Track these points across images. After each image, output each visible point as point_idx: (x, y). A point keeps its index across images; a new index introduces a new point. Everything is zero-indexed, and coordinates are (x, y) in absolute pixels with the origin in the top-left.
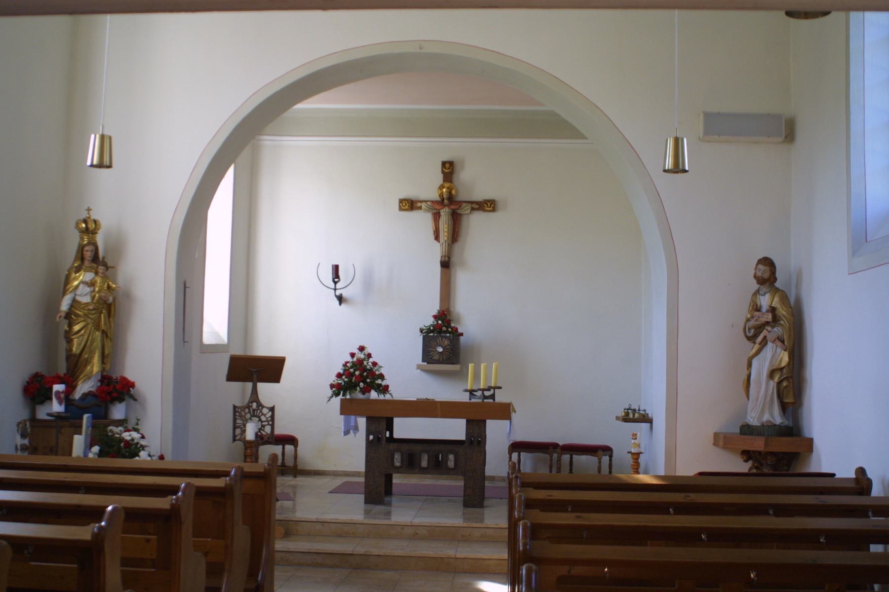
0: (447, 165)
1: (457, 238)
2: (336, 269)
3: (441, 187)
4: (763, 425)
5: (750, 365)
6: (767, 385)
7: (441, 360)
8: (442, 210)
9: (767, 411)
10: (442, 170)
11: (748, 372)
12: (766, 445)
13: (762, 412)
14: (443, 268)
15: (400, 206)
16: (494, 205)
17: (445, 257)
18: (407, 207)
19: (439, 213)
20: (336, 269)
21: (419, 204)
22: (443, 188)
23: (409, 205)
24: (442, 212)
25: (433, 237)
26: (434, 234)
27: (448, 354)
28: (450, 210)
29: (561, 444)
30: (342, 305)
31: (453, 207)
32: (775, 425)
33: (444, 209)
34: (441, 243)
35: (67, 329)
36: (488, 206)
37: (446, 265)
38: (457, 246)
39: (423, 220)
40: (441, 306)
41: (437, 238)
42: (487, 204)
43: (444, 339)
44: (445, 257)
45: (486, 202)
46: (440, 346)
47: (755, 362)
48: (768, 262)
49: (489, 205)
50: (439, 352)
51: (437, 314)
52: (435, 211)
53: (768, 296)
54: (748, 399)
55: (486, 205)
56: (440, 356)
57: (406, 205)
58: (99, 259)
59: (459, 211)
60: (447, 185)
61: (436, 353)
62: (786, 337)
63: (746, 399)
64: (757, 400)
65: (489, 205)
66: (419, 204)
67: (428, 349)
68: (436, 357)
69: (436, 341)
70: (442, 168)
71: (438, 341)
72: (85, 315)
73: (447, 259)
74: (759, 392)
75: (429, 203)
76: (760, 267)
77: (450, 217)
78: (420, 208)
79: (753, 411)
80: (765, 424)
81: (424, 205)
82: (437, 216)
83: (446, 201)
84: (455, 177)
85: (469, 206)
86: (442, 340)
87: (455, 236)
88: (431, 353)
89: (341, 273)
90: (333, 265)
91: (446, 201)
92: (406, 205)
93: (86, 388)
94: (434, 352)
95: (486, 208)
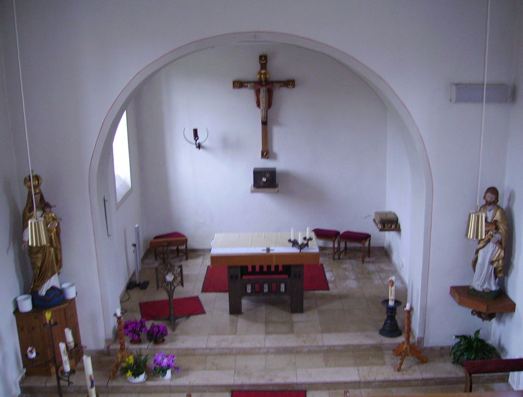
2: (195, 131)
4: (484, 291)
5: (477, 252)
6: (488, 267)
9: (487, 282)
10: (260, 62)
11: (476, 256)
12: (487, 309)
13: (484, 283)
16: (294, 84)
20: (195, 131)
23: (239, 84)
24: (261, 90)
26: (257, 103)
29: (342, 232)
30: (201, 149)
32: (491, 291)
36: (290, 83)
37: (264, 123)
39: (248, 94)
41: (259, 105)
47: (481, 252)
48: (493, 191)
51: (254, 90)
53: (492, 212)
54: (475, 271)
58: (36, 352)
60: (263, 71)
62: (503, 242)
63: (472, 271)
64: (481, 275)
66: (246, 85)
70: (260, 60)
75: (252, 84)
76: (489, 194)
78: (247, 86)
79: (478, 280)
80: (485, 291)
81: (249, 85)
82: (258, 93)
84: (269, 65)
87: (269, 104)
89: (199, 134)
90: (194, 130)
93: (45, 287)
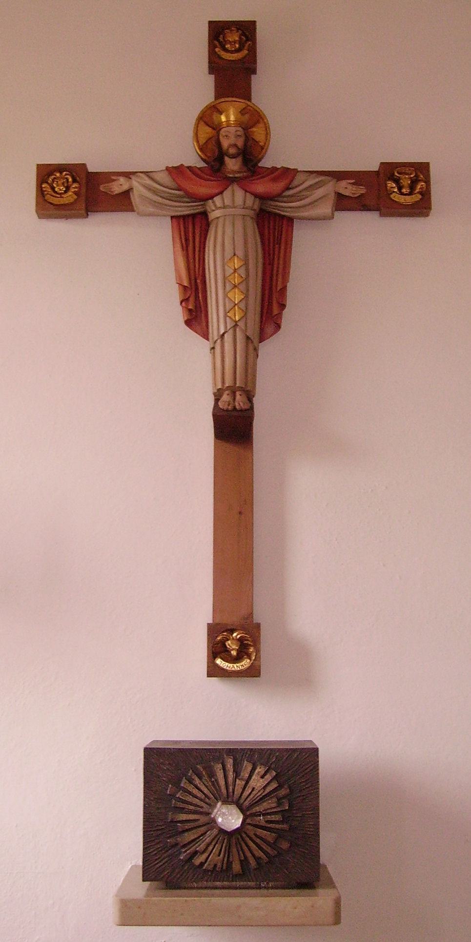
0: (233, 36)
1: (280, 315)
3: (207, 117)
7: (236, 867)
8: (217, 200)
10: (212, 54)
14: (229, 447)
15: (41, 192)
17: (234, 394)
18: (70, 197)
19: (204, 214)
21: (119, 186)
22: (221, 114)
25: (178, 314)
27: (270, 836)
28: (250, 200)
31: (261, 187)
33: (227, 194)
34: (214, 333)
35: (402, 191)
38: (268, 350)
40: (217, 608)
42: (397, 181)
43: (247, 767)
44: (234, 394)
45: (390, 171)
46: (226, 802)
49: (406, 182)
50: (222, 831)
52: (185, 209)
55: (391, 184)
56: (229, 851)
57: (68, 189)
59: (285, 208)
61: (215, 831)
65: (406, 182)
67: (170, 816)
68: (215, 857)
69: (212, 774)
71: (220, 775)
72: (169, 764)
73: (240, 401)
74: (248, 846)
77: (251, 227)
83: (232, 165)
85: (329, 188)
86: (237, 773)
88: (189, 837)
91: (232, 165)
92: (68, 189)
94: (203, 829)
95: (396, 197)
